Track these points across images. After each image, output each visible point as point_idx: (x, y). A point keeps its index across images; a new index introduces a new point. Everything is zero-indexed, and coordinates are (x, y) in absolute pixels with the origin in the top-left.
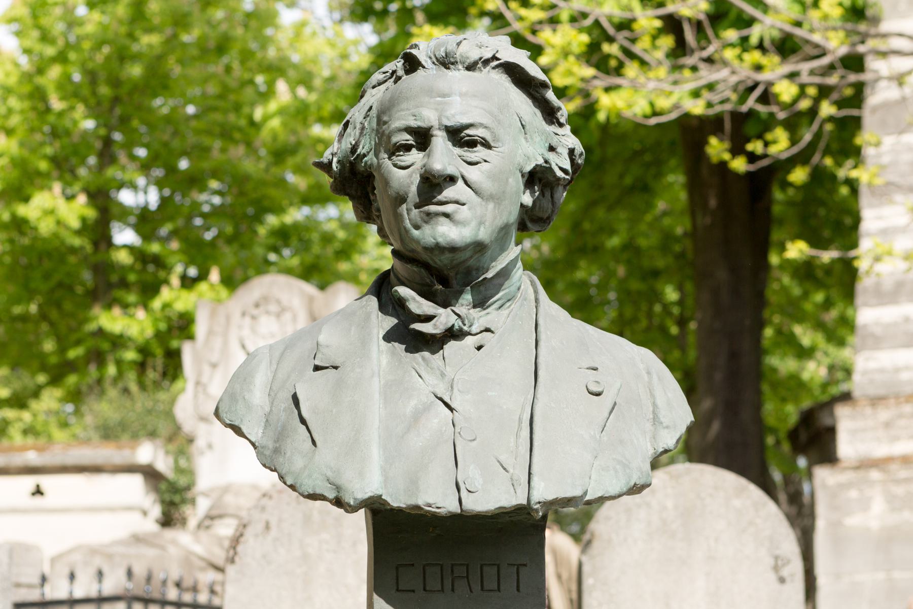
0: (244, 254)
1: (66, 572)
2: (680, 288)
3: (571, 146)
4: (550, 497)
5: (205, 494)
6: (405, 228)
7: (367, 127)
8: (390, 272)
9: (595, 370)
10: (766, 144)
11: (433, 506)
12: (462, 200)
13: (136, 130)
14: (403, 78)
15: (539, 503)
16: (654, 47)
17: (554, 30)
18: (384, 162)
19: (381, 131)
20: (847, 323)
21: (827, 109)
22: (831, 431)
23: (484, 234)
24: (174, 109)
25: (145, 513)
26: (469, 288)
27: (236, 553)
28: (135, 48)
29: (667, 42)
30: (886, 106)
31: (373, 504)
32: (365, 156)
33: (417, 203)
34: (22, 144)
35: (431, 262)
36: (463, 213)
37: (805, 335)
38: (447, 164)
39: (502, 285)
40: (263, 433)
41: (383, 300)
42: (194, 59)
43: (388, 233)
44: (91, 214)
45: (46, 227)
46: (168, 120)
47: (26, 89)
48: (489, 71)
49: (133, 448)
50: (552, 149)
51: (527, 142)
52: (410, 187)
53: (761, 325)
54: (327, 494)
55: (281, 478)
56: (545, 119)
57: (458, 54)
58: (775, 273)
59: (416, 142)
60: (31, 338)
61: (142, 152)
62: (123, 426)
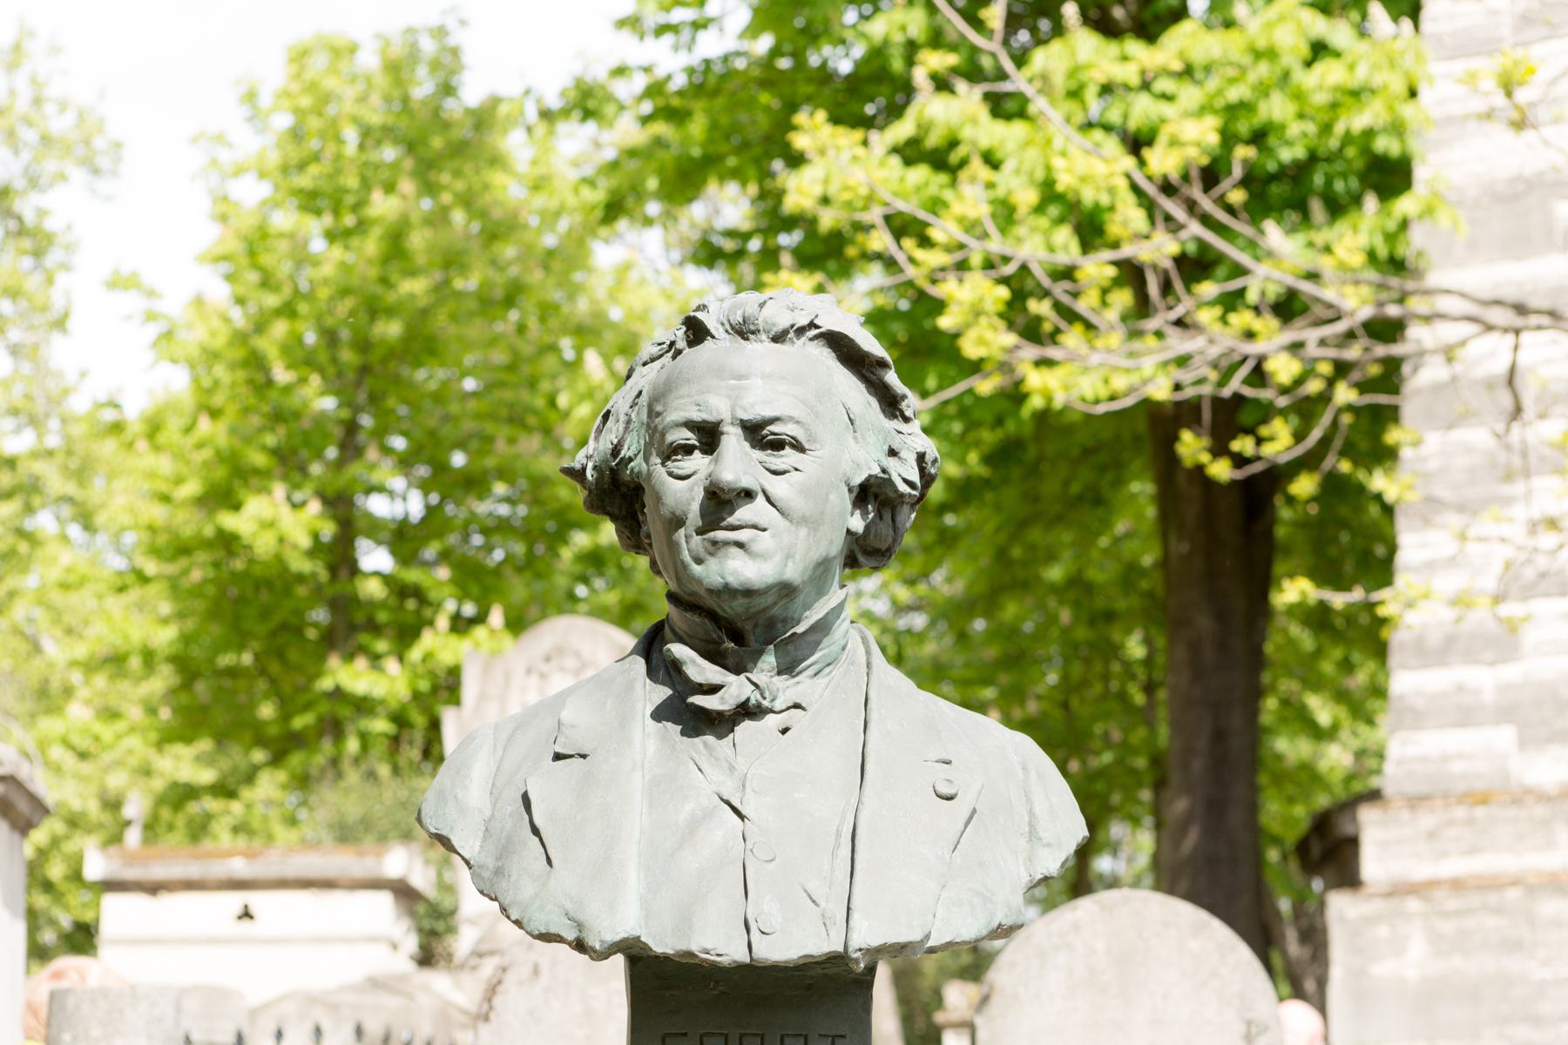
0: (539, 586)
1: (271, 1028)
2: (1148, 641)
3: (921, 450)
4: (875, 942)
5: (472, 922)
6: (683, 562)
7: (634, 420)
8: (663, 626)
9: (947, 763)
10: (1259, 441)
11: (712, 952)
12: (763, 524)
13: (393, 411)
14: (684, 352)
15: (860, 950)
16: (1104, 303)
17: (961, 280)
18: (655, 469)
19: (652, 425)
20: (1378, 691)
21: (1344, 394)
22: (1353, 843)
23: (793, 572)
24: (445, 384)
25: (395, 946)
26: (772, 647)
27: (491, 1008)
28: (391, 298)
29: (1123, 298)
30: (1437, 388)
31: (631, 948)
32: (631, 460)
33: (699, 528)
34: (233, 431)
35: (718, 610)
36: (762, 541)
37: (1323, 711)
38: (741, 474)
39: (818, 643)
40: (481, 846)
41: (654, 662)
42: (471, 314)
43: (661, 568)
44: (328, 530)
45: (264, 545)
46: (439, 398)
47: (239, 354)
48: (804, 344)
49: (379, 855)
50: (893, 453)
51: (857, 443)
52: (689, 504)
53: (1256, 693)
54: (564, 934)
55: (503, 910)
56: (884, 411)
57: (760, 319)
58: (1280, 621)
59: (699, 442)
60: (242, 698)
61: (399, 443)
62: (366, 824)
